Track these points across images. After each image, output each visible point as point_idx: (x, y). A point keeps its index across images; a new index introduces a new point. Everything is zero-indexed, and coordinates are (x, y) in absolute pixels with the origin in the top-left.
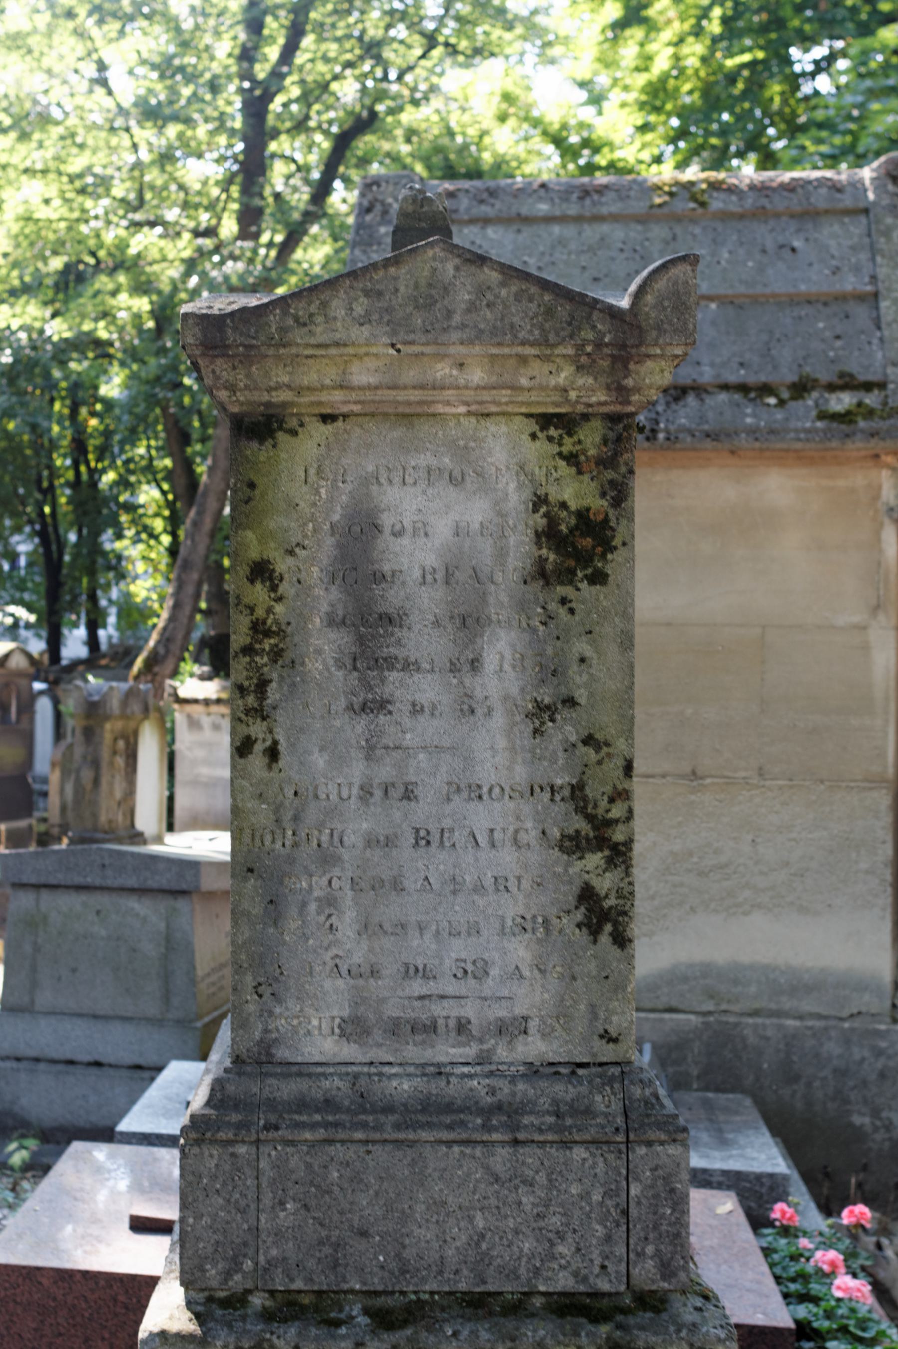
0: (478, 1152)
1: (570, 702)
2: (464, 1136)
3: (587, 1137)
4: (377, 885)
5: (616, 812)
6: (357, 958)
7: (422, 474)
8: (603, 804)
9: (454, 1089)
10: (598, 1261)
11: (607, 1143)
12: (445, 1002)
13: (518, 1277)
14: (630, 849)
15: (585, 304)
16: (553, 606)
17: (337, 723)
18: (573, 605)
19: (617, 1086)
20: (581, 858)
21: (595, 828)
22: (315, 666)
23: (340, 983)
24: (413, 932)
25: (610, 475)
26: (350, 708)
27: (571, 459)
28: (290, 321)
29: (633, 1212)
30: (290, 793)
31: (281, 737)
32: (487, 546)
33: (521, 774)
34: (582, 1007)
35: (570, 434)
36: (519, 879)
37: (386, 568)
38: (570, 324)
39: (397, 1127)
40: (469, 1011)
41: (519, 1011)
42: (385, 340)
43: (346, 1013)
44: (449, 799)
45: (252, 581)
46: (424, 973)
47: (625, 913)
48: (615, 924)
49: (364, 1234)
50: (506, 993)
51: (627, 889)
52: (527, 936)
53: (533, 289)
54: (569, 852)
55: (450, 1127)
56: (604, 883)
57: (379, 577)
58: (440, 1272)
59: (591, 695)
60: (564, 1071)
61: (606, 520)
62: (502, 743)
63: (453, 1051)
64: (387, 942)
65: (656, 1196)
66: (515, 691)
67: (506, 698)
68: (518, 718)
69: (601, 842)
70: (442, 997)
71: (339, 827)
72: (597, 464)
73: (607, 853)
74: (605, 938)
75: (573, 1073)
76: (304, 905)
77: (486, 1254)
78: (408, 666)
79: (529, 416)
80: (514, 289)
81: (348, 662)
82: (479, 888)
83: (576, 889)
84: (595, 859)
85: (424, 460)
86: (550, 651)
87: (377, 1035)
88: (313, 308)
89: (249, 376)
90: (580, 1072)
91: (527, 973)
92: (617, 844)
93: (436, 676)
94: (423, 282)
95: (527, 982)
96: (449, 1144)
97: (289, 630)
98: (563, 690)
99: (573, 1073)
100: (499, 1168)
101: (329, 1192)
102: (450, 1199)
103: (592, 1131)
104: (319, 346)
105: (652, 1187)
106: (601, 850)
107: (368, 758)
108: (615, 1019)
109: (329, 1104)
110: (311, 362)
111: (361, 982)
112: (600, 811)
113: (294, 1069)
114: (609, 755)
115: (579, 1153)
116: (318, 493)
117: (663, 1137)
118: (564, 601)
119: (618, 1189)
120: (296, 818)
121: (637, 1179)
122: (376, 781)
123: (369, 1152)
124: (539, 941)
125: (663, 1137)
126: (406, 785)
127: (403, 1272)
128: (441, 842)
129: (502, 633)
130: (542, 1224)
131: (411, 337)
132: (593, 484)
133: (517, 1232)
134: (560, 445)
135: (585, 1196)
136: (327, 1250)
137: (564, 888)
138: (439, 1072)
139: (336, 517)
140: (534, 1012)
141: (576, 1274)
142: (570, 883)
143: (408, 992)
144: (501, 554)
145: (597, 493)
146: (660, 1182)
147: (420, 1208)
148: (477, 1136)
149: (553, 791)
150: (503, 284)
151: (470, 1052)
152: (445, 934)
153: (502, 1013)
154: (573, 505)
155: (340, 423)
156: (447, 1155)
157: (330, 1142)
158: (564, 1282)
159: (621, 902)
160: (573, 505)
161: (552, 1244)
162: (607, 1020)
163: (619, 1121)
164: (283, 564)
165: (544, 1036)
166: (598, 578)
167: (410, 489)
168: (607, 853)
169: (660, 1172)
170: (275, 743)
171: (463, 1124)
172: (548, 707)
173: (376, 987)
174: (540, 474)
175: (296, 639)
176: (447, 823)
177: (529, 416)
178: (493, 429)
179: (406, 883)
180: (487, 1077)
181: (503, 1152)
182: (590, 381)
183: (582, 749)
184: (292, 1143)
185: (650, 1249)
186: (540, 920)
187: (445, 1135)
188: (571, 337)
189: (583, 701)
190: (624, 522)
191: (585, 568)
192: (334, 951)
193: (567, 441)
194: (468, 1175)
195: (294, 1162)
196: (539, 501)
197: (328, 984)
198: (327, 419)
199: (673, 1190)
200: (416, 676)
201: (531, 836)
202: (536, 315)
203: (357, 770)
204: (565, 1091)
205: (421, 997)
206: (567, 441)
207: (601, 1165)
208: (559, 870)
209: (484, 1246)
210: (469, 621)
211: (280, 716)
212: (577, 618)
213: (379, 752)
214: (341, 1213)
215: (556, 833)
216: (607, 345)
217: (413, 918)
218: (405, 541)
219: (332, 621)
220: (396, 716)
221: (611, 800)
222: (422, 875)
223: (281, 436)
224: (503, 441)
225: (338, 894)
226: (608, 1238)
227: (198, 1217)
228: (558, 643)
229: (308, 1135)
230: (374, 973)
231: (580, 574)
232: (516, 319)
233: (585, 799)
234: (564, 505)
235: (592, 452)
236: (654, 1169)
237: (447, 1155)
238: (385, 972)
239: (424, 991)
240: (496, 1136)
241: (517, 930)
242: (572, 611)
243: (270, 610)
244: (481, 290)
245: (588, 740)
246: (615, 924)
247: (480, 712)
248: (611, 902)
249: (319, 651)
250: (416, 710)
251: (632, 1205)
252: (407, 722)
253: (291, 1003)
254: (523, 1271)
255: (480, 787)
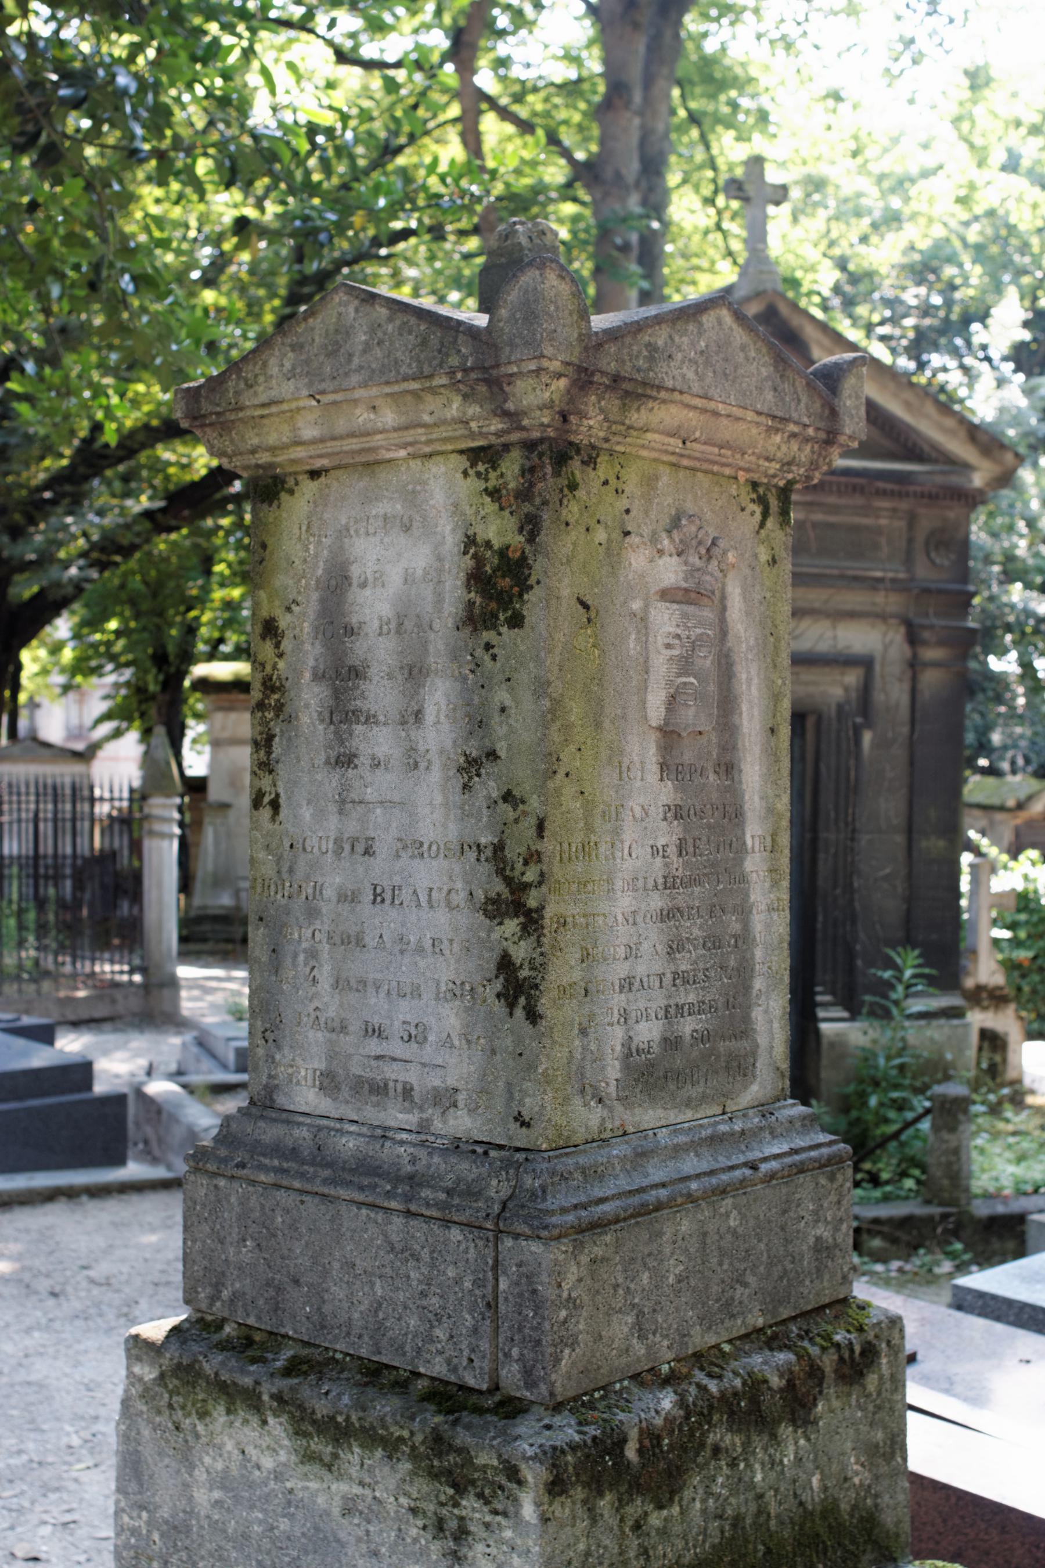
0: (380, 1217)
1: (492, 755)
2: (370, 1199)
3: (462, 1219)
4: (346, 940)
5: (530, 876)
6: (331, 1013)
7: (380, 523)
8: (519, 866)
9: (389, 1153)
10: (466, 1353)
11: (480, 1228)
12: (395, 1066)
13: (404, 1354)
14: (542, 917)
15: (451, 328)
16: (479, 652)
17: (319, 777)
18: (495, 651)
19: (512, 1171)
20: (501, 924)
21: (512, 893)
22: (305, 719)
23: (319, 1034)
24: (371, 990)
25: (527, 508)
26: (327, 762)
27: (494, 494)
28: (242, 385)
29: (502, 1308)
30: (287, 845)
31: (281, 791)
32: (427, 592)
33: (453, 832)
34: (501, 1084)
35: (494, 468)
36: (451, 941)
37: (354, 620)
38: (440, 351)
39: (325, 1182)
40: (412, 1076)
41: (451, 1082)
42: (305, 392)
43: (323, 1066)
44: (398, 856)
45: (263, 638)
46: (376, 1032)
47: (536, 987)
48: (529, 998)
49: (296, 1282)
50: (440, 1061)
51: (539, 960)
52: (457, 1003)
53: (413, 321)
54: (491, 918)
55: (361, 1188)
56: (520, 952)
57: (350, 631)
58: (348, 1334)
59: (510, 748)
60: (480, 1150)
61: (524, 558)
62: (439, 799)
63: (400, 1116)
64: (353, 997)
65: (521, 1295)
66: (448, 744)
67: (442, 751)
68: (451, 773)
69: (518, 908)
70: (394, 1059)
71: (320, 880)
72: (516, 498)
73: (522, 919)
74: (519, 1013)
75: (486, 1153)
76: (295, 956)
77: (381, 1323)
78: (370, 719)
79: (461, 452)
80: (398, 322)
81: (327, 715)
82: (420, 950)
83: (496, 955)
84: (512, 926)
85: (383, 508)
86: (476, 700)
87: (345, 1093)
88: (257, 370)
89: (232, 441)
90: (493, 1153)
91: (457, 1043)
92: (530, 910)
93: (390, 729)
94: (332, 328)
95: (456, 1052)
96: (360, 1204)
97: (287, 684)
98: (488, 744)
99: (486, 1153)
100: (394, 1238)
101: (275, 1236)
102: (358, 1262)
103: (468, 1212)
104: (263, 405)
105: (517, 1284)
106: (517, 916)
107: (341, 812)
108: (527, 1100)
109: (294, 1153)
110: (265, 421)
111: (334, 1036)
112: (517, 873)
113: (284, 1115)
114: (525, 813)
115: (455, 1234)
116: (307, 550)
117: (527, 1231)
118: (488, 647)
119: (485, 1279)
120: (291, 871)
121: (505, 1273)
122: (346, 835)
123: (302, 1202)
124: (467, 1010)
125: (527, 1231)
126: (367, 839)
127: (323, 1327)
128: (430, 901)
129: (439, 682)
130: (425, 1303)
131: (323, 386)
132: (513, 519)
133: (405, 1308)
134: (487, 480)
135: (459, 1281)
136: (272, 1293)
137: (487, 955)
138: (383, 1134)
139: (320, 572)
140: (460, 1085)
141: (448, 1362)
142: (492, 950)
143: (366, 1051)
144: (439, 600)
145: (516, 528)
146: (524, 1280)
147: (336, 1265)
148: (379, 1201)
149: (480, 851)
150: (390, 320)
151: (410, 1119)
152: (394, 993)
153: (437, 1083)
154: (496, 544)
155: (323, 479)
156: (357, 1216)
157: (277, 1186)
158: (438, 1368)
159: (533, 974)
160: (496, 544)
161: (432, 1327)
162: (521, 1102)
163: (497, 1208)
164: (284, 621)
165: (472, 1111)
166: (516, 621)
167: (372, 539)
168: (522, 919)
169: (524, 1269)
170: (278, 795)
171: (373, 1187)
172: (475, 760)
173: (347, 1042)
174: (469, 511)
175: (292, 694)
176: (397, 880)
177: (461, 452)
178: (434, 470)
179: (367, 940)
180: (415, 1145)
181: (398, 1221)
182: (478, 409)
183: (503, 807)
184: (253, 1183)
185: (515, 1352)
186: (467, 987)
187: (360, 1197)
188: (441, 366)
189: (503, 754)
190: (540, 558)
191: (505, 610)
192: (316, 1003)
193: (493, 475)
194: (372, 1240)
195: (253, 1202)
196: (470, 541)
197: (311, 1034)
198: (314, 474)
199: (534, 1292)
200: (376, 729)
201: (460, 898)
202: (415, 347)
203: (332, 823)
204: (466, 1169)
205: (378, 1058)
206: (493, 475)
207: (472, 1250)
208: (483, 935)
209: (381, 1315)
210: (415, 671)
211: (280, 769)
212: (498, 664)
213: (349, 806)
214: (283, 1258)
215: (480, 895)
216: (472, 369)
217: (371, 976)
218: (368, 592)
219: (317, 677)
220: (360, 769)
221: (526, 863)
222: (378, 932)
223: (284, 496)
224: (442, 481)
225: (319, 947)
226: (475, 1330)
227: (194, 1241)
228: (483, 692)
229: (262, 1178)
230: (343, 1029)
231: (502, 617)
232: (399, 354)
233: (504, 860)
234: (488, 544)
235: (512, 485)
236: (519, 1265)
237: (357, 1216)
238: (351, 1028)
239: (379, 1052)
240: (394, 1204)
241: (449, 996)
242: (494, 658)
243: (275, 667)
244: (374, 328)
245: (508, 797)
246: (529, 998)
247: (423, 765)
248: (524, 973)
249: (307, 706)
250: (376, 764)
251: (501, 1300)
252: (368, 776)
253: (286, 1050)
254: (408, 1348)
255: (421, 844)
